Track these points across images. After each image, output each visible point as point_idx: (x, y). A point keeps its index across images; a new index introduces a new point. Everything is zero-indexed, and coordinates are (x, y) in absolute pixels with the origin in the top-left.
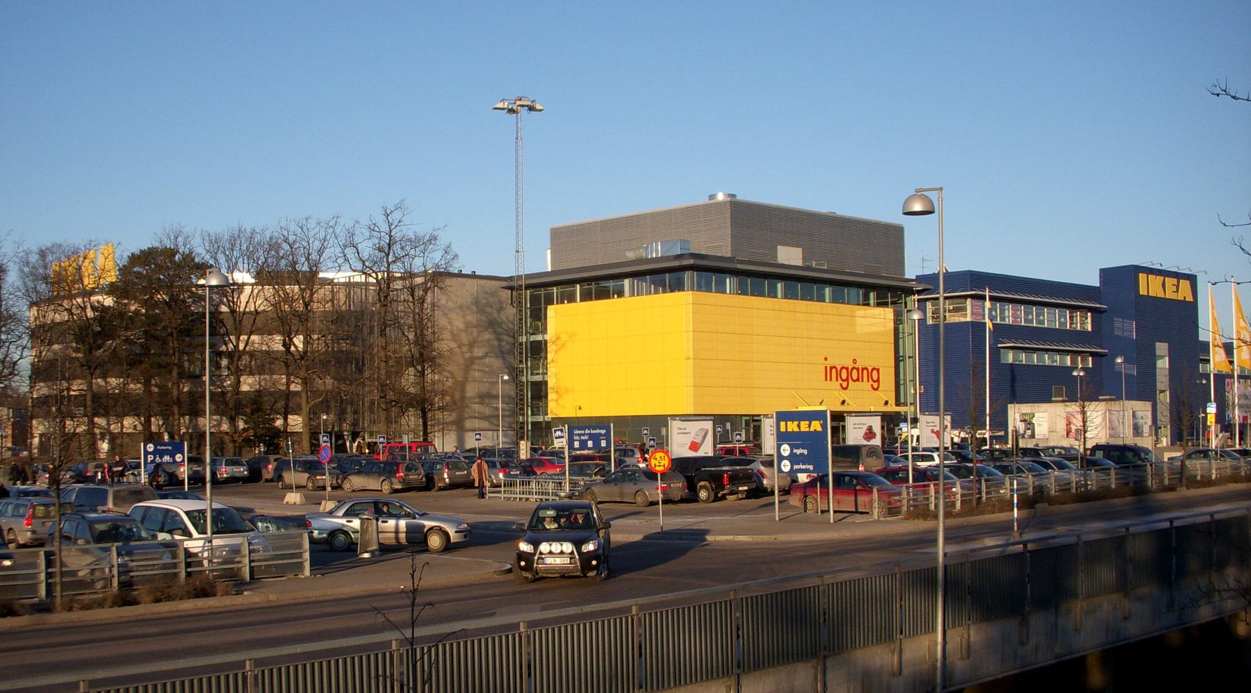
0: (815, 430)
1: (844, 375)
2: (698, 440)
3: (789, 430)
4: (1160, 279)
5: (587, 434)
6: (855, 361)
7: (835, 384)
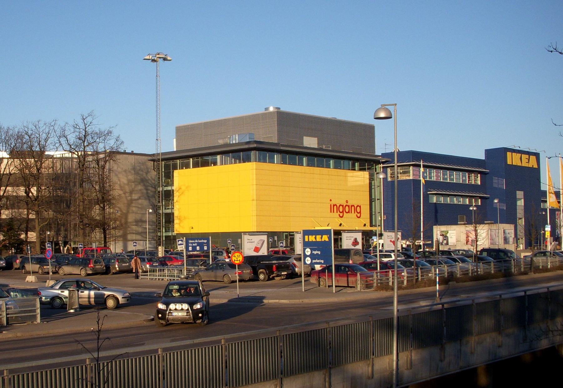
0: (325, 240)
1: (341, 209)
2: (259, 246)
3: (310, 240)
4: (519, 155)
5: (196, 243)
6: (347, 202)
7: (336, 215)
